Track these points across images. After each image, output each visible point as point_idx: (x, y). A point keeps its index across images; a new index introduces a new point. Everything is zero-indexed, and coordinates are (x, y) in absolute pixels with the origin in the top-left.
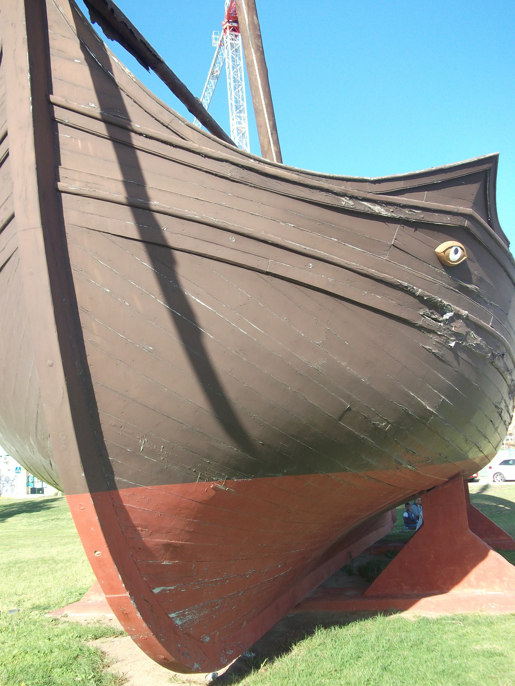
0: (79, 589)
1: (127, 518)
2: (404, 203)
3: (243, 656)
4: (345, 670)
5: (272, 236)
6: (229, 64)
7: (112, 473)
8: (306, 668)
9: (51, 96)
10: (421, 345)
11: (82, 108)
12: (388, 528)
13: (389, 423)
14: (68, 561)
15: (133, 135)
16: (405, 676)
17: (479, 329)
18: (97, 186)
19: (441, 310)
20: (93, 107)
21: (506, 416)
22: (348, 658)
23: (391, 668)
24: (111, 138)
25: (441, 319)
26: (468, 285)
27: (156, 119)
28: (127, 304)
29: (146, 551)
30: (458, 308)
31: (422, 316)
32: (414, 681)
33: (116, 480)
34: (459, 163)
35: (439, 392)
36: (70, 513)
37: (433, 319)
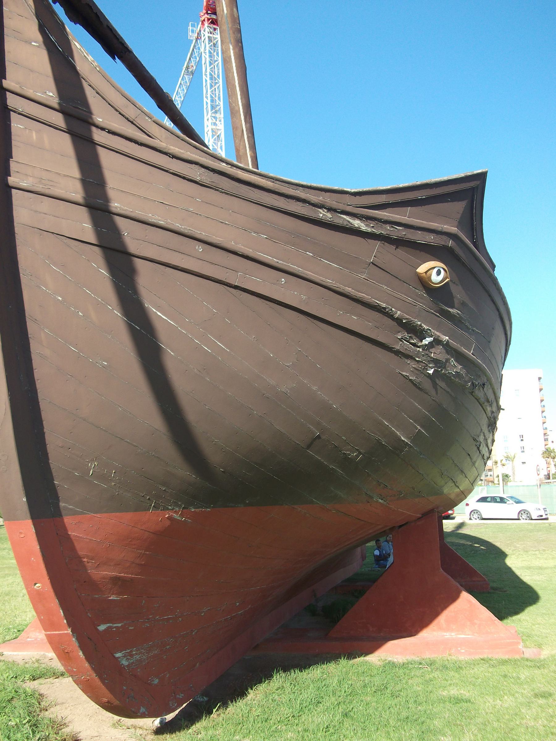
0: (18, 626)
1: (73, 549)
2: (386, 218)
3: (195, 701)
4: (303, 716)
5: (242, 247)
6: (206, 59)
7: (57, 498)
8: (262, 713)
9: (4, 81)
10: (398, 371)
11: (39, 96)
12: (355, 567)
13: (360, 453)
14: (7, 594)
15: (94, 129)
16: (367, 723)
17: (460, 357)
18: (51, 183)
19: (421, 334)
20: (51, 95)
21: (484, 450)
22: (308, 703)
23: (352, 714)
24: (70, 131)
25: (420, 344)
26: (449, 309)
27: (120, 113)
28: (80, 314)
29: (91, 584)
30: (438, 333)
31: (400, 340)
32: (376, 728)
33: (61, 507)
34: (445, 178)
35: (415, 421)
36: (9, 543)
37: (411, 343)
